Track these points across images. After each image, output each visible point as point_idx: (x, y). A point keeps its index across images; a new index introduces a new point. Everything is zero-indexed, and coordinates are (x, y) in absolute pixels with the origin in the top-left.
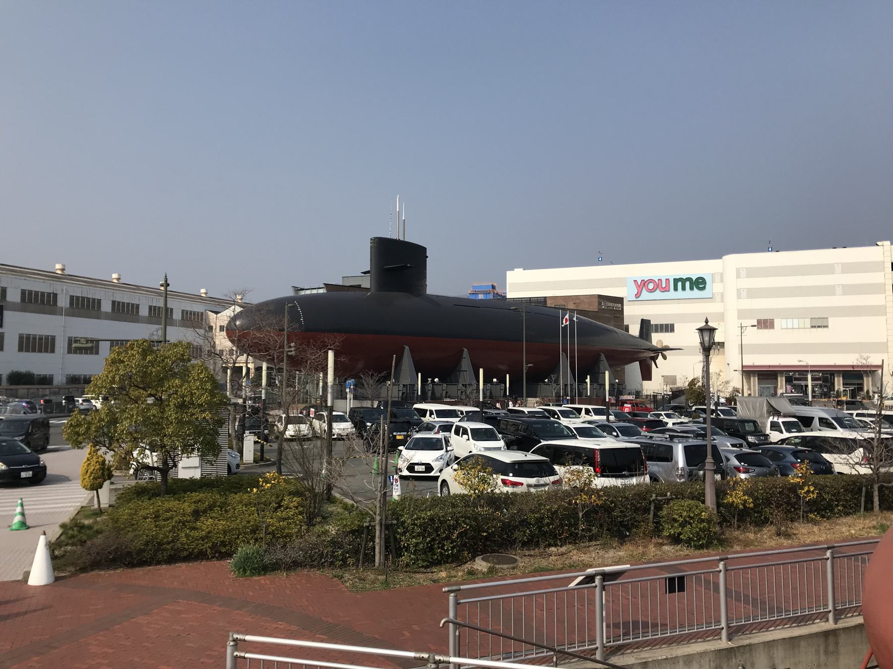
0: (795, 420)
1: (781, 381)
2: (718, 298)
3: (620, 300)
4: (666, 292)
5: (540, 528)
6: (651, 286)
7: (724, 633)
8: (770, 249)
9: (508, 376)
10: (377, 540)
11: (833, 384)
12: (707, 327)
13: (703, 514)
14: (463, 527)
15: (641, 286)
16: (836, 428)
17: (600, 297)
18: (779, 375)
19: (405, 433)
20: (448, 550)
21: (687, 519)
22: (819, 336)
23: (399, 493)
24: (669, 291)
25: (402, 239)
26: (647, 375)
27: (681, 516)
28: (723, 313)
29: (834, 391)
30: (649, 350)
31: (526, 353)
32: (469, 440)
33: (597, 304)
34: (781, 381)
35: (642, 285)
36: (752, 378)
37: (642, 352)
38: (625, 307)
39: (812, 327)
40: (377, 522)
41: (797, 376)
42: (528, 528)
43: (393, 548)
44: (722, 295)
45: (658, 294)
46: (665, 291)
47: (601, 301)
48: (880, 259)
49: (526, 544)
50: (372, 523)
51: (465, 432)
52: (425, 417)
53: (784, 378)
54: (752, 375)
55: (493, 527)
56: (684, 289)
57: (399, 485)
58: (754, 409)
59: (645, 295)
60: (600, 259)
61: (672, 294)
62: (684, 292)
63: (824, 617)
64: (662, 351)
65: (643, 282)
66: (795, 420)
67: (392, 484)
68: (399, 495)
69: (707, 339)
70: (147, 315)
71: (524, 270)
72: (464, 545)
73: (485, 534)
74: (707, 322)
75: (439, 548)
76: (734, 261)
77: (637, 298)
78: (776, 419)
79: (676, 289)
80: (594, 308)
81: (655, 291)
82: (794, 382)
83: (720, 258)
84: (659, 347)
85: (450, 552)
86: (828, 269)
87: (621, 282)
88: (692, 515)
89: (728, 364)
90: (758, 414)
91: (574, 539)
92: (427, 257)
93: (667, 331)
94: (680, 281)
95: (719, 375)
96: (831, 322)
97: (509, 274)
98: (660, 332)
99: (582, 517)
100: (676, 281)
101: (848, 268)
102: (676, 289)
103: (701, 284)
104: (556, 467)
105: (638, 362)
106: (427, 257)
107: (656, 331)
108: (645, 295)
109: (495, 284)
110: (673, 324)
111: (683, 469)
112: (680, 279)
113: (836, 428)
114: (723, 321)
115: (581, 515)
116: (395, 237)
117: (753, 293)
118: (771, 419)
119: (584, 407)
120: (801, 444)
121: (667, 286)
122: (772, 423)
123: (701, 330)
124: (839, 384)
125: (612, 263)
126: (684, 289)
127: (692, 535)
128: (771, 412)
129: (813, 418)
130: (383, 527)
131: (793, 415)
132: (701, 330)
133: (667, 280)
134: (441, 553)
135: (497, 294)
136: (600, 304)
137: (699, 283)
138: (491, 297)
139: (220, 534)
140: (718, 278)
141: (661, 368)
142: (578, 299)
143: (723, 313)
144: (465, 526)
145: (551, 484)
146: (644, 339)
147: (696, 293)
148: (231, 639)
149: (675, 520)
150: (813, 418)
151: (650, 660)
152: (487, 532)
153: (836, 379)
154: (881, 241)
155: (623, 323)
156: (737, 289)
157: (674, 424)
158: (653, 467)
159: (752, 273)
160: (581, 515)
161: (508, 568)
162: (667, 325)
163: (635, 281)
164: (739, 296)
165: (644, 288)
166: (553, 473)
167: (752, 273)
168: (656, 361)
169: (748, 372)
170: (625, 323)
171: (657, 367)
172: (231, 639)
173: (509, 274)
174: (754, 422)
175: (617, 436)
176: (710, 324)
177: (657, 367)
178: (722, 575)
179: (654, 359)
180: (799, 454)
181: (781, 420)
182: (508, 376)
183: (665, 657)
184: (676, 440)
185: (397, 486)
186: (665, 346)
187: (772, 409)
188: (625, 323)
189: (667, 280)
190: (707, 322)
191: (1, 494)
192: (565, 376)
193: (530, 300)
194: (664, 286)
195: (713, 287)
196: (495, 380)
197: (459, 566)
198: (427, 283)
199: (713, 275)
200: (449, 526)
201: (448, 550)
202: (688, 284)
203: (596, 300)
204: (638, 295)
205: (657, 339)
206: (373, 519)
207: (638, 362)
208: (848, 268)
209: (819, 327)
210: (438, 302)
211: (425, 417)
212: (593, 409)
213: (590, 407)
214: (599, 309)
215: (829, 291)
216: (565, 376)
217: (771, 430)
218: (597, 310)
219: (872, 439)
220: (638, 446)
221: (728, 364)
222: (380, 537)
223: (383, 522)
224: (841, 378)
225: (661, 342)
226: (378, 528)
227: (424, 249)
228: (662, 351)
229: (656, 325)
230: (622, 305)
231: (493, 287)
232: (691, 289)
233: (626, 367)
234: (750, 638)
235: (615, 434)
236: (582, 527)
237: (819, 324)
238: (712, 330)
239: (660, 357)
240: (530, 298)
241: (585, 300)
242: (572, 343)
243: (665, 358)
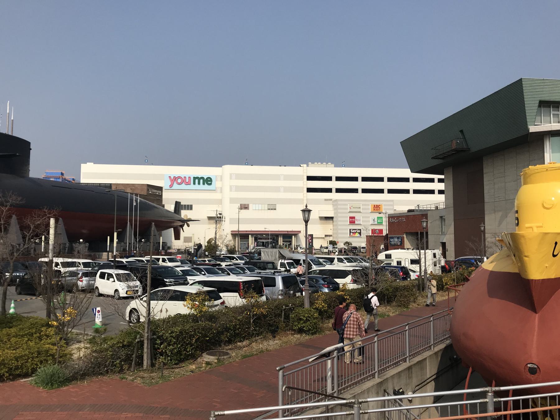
0: (292, 261)
1: (251, 240)
2: (219, 190)
3: (160, 189)
4: (188, 185)
5: (234, 331)
6: (179, 181)
7: (376, 374)
8: (247, 164)
9: (109, 237)
10: (145, 350)
11: (278, 241)
12: (307, 209)
13: (315, 314)
14: (197, 335)
15: (173, 181)
16: (180, 270)
17: (148, 185)
18: (279, 236)
19: (57, 279)
20: (190, 351)
21: (308, 318)
22: (271, 214)
23: (101, 320)
24: (190, 184)
25: (10, 134)
27: (304, 317)
28: (221, 199)
29: (278, 245)
31: (116, 223)
32: (114, 281)
33: (146, 191)
34: (251, 240)
35: (174, 180)
36: (237, 238)
37: (174, 222)
38: (164, 193)
39: (269, 209)
40: (146, 337)
41: (260, 237)
42: (228, 332)
43: (155, 354)
44: (221, 188)
45: (183, 186)
46: (188, 184)
47: (149, 188)
48: (301, 173)
49: (230, 342)
50: (142, 339)
51: (110, 276)
53: (254, 238)
54: (237, 236)
55: (211, 334)
56: (199, 184)
57: (101, 315)
58: (272, 256)
59: (175, 186)
60: (146, 161)
61: (192, 186)
62: (194, 186)
63: (405, 360)
64: (186, 221)
65: (175, 178)
66: (292, 261)
67: (95, 314)
68: (100, 322)
69: (306, 216)
71: (94, 164)
72: (197, 347)
73: (208, 338)
74: (306, 206)
75: (184, 350)
76: (228, 169)
78: (283, 261)
79: (194, 183)
80: (144, 193)
81: (181, 184)
82: (258, 240)
83: (221, 167)
84: (185, 219)
85: (191, 352)
86: (276, 177)
87: (161, 177)
88: (310, 316)
90: (273, 258)
91: (249, 336)
92: (31, 149)
93: (188, 209)
95: (226, 236)
96: (278, 207)
97: (83, 166)
98: (184, 210)
99: (253, 322)
100: (195, 178)
101: (288, 178)
102: (194, 183)
103: (210, 182)
104: (221, 295)
105: (173, 228)
106: (31, 149)
107: (185, 209)
108: (175, 186)
109: (63, 172)
110: (192, 205)
111: (282, 290)
112: (197, 178)
113: (180, 270)
114: (221, 204)
115: (252, 321)
116: (4, 132)
117: (239, 189)
118: (280, 261)
119: (161, 257)
120: (319, 273)
121: (189, 182)
122: (281, 263)
123: (303, 211)
124: (281, 241)
125: (152, 164)
126: (199, 184)
127: (310, 327)
128: (280, 257)
129: (300, 260)
130: (149, 340)
131: (291, 258)
132: (303, 211)
133: (189, 177)
134: (185, 353)
135: (65, 179)
136: (148, 190)
137: (208, 181)
138: (60, 180)
139: (12, 360)
140: (219, 178)
141: (186, 232)
142: (133, 186)
143: (221, 199)
144: (199, 334)
145: (220, 305)
146: (177, 214)
147: (206, 187)
148: (212, 416)
149: (301, 319)
150: (300, 260)
151: (356, 394)
152: (209, 337)
153: (279, 238)
154: (302, 164)
155: (162, 203)
156: (230, 186)
157: (226, 266)
158: (266, 290)
159: (239, 177)
160: (252, 321)
161: (227, 358)
162: (188, 206)
163: (170, 177)
164: (231, 190)
165: (175, 182)
166: (220, 298)
167: (239, 177)
168: (183, 228)
169: (235, 235)
170: (163, 204)
171: (184, 232)
172: (212, 416)
173: (83, 166)
174: (273, 263)
175: (205, 274)
176: (309, 208)
177: (184, 232)
178: (376, 344)
179: (182, 226)
180: (325, 279)
181: (286, 262)
182: (109, 237)
183: (361, 391)
184: (276, 274)
185: (99, 315)
186: (189, 219)
187: (281, 256)
188: (163, 204)
189: (189, 177)
190: (306, 206)
192: (130, 239)
193: (100, 185)
194: (187, 181)
195: (216, 184)
196: (81, 240)
197: (195, 361)
198: (30, 169)
199: (216, 176)
200: (191, 335)
201: (190, 351)
202: (201, 181)
203: (146, 188)
204: (171, 186)
205: (184, 214)
206: (142, 336)
207: (173, 228)
208: (288, 178)
209: (272, 209)
210: (36, 182)
212: (168, 258)
213: (166, 257)
214: (147, 194)
215: (276, 189)
216: (130, 239)
217: (280, 267)
218: (146, 194)
220: (260, 278)
222: (147, 348)
223: (149, 337)
224: (282, 238)
225: (186, 216)
226: (146, 342)
227: (29, 143)
228: (186, 221)
229: (185, 205)
230: (162, 192)
231: (62, 174)
232: (204, 184)
233: (163, 232)
234: (384, 375)
235: (203, 273)
236: (252, 328)
237: (272, 208)
238: (309, 211)
239: (186, 225)
240: (100, 184)
241: (139, 187)
242: (136, 215)
243: (188, 226)
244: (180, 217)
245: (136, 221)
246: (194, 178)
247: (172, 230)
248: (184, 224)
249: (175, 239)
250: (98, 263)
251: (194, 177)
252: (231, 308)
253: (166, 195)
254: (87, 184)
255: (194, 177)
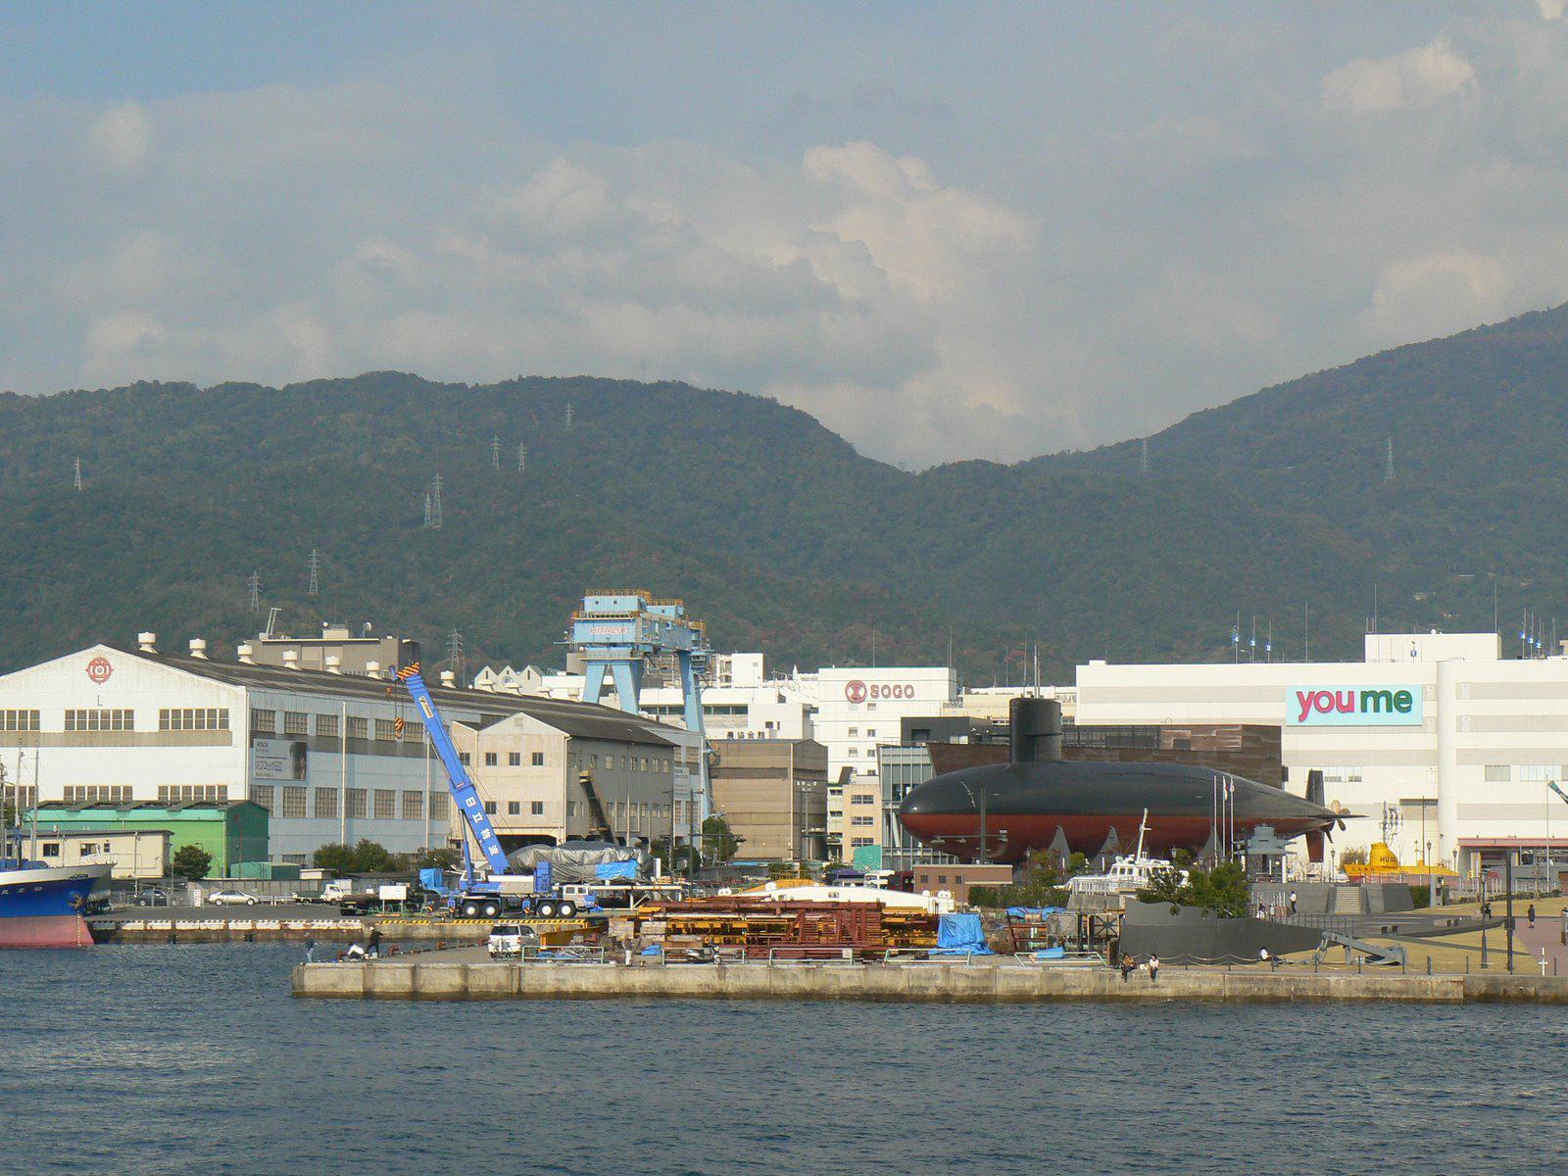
26: (1316, 854)
30: (1319, 817)
35: (1309, 701)
45: (1335, 716)
52: (799, 672)
56: (1377, 709)
61: (1356, 717)
70: (62, 729)
77: (1300, 721)
79: (1364, 709)
84: (1336, 811)
87: (1274, 694)
89: (1442, 836)
92: (792, 406)
94: (1370, 695)
100: (1365, 695)
102: (1364, 709)
106: (792, 406)
112: (1372, 693)
117: (1480, 724)
126: (1377, 709)
133: (1351, 694)
168: (1331, 832)
169: (1467, 849)
171: (1331, 842)
177: (1331, 842)
179: (1328, 829)
191: (2, 1020)
195: (1422, 708)
202: (1383, 701)
204: (1302, 718)
211: (799, 672)
219: (1076, 869)
221: (1442, 836)
232: (1389, 710)
243: (1343, 828)
244: (1322, 808)
245: (1228, 814)
246: (1352, 710)
247: (1302, 840)
248: (1333, 824)
249: (207, 858)
250: (1281, 864)
251: (1362, 692)
252: (918, 477)
253: (1288, 743)
254: (1115, 734)
255: (1362, 692)
